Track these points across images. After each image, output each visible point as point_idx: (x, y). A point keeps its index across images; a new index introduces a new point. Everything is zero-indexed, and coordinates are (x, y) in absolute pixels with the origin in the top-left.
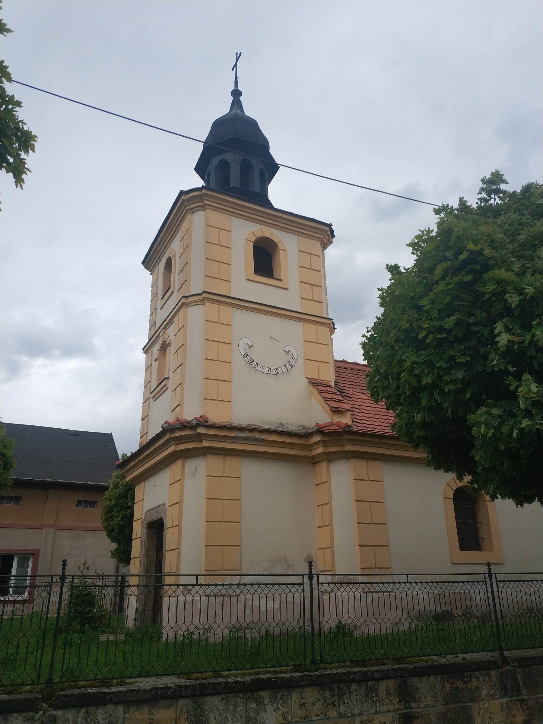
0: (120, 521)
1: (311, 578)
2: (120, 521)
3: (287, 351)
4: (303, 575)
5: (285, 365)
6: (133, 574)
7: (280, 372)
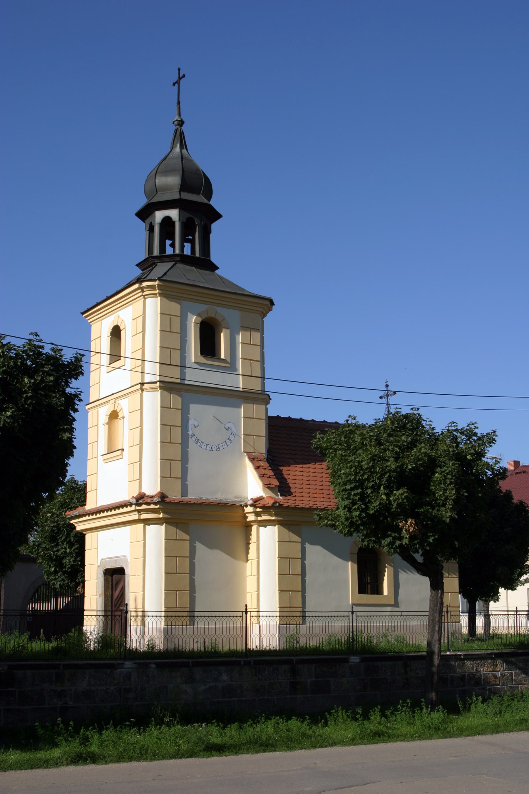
0: (363, 450)
1: (353, 613)
2: (363, 450)
3: (227, 428)
4: (349, 612)
5: (225, 442)
6: (100, 533)
7: (221, 448)
